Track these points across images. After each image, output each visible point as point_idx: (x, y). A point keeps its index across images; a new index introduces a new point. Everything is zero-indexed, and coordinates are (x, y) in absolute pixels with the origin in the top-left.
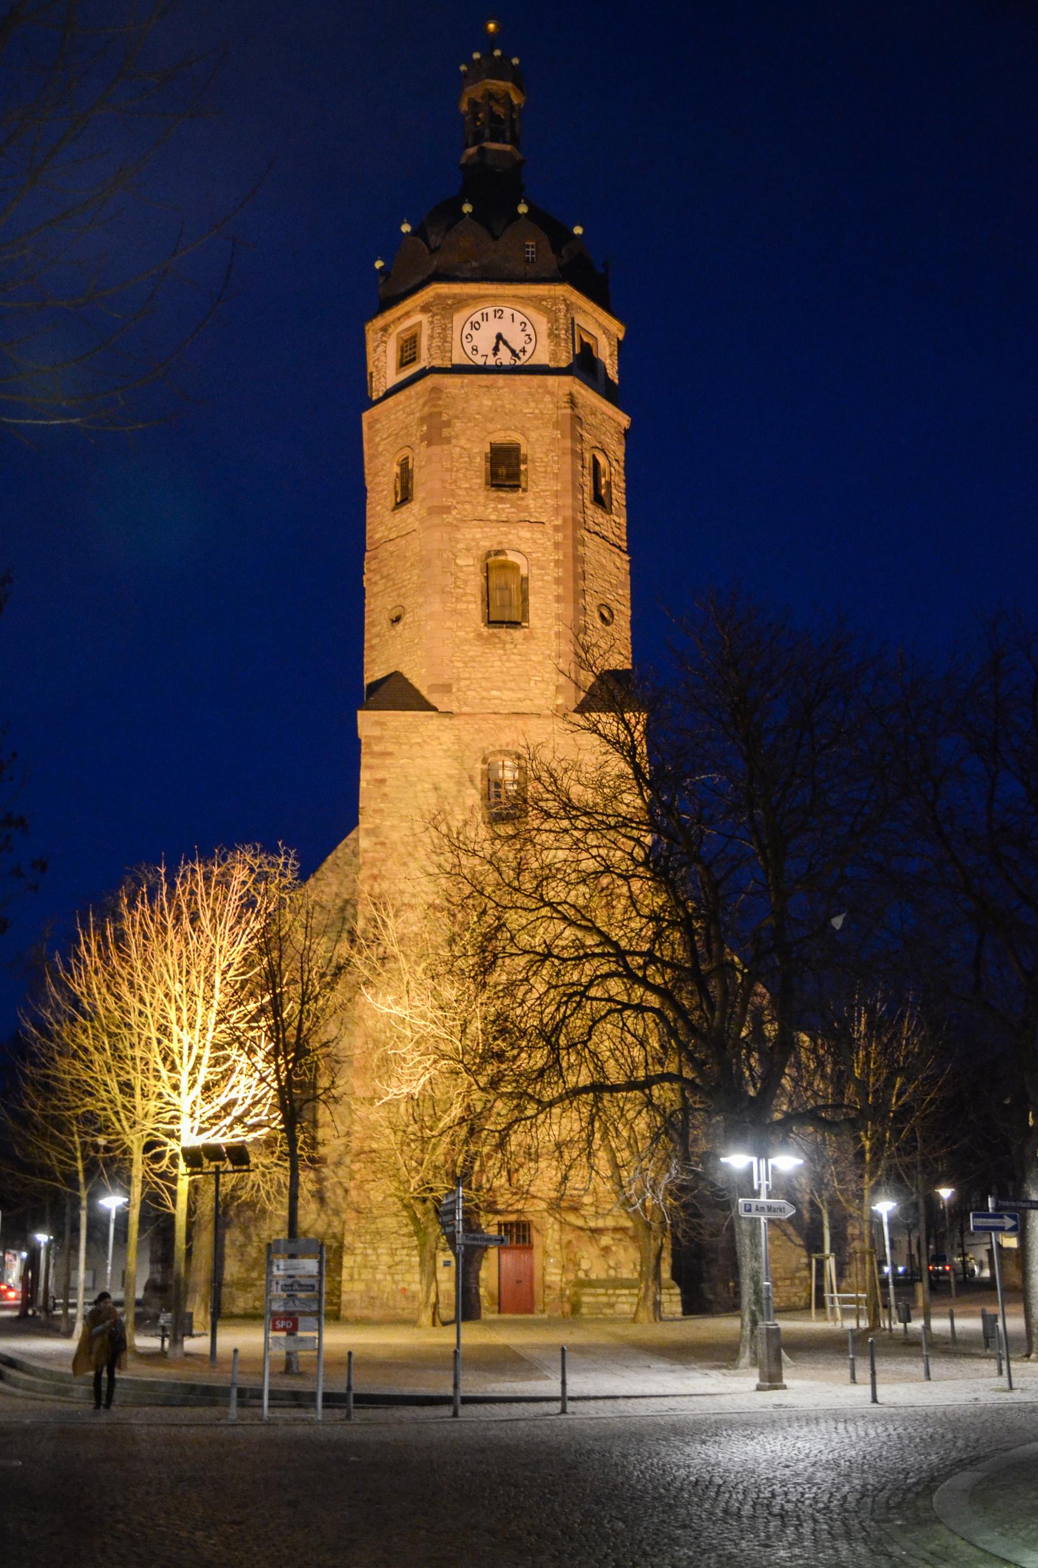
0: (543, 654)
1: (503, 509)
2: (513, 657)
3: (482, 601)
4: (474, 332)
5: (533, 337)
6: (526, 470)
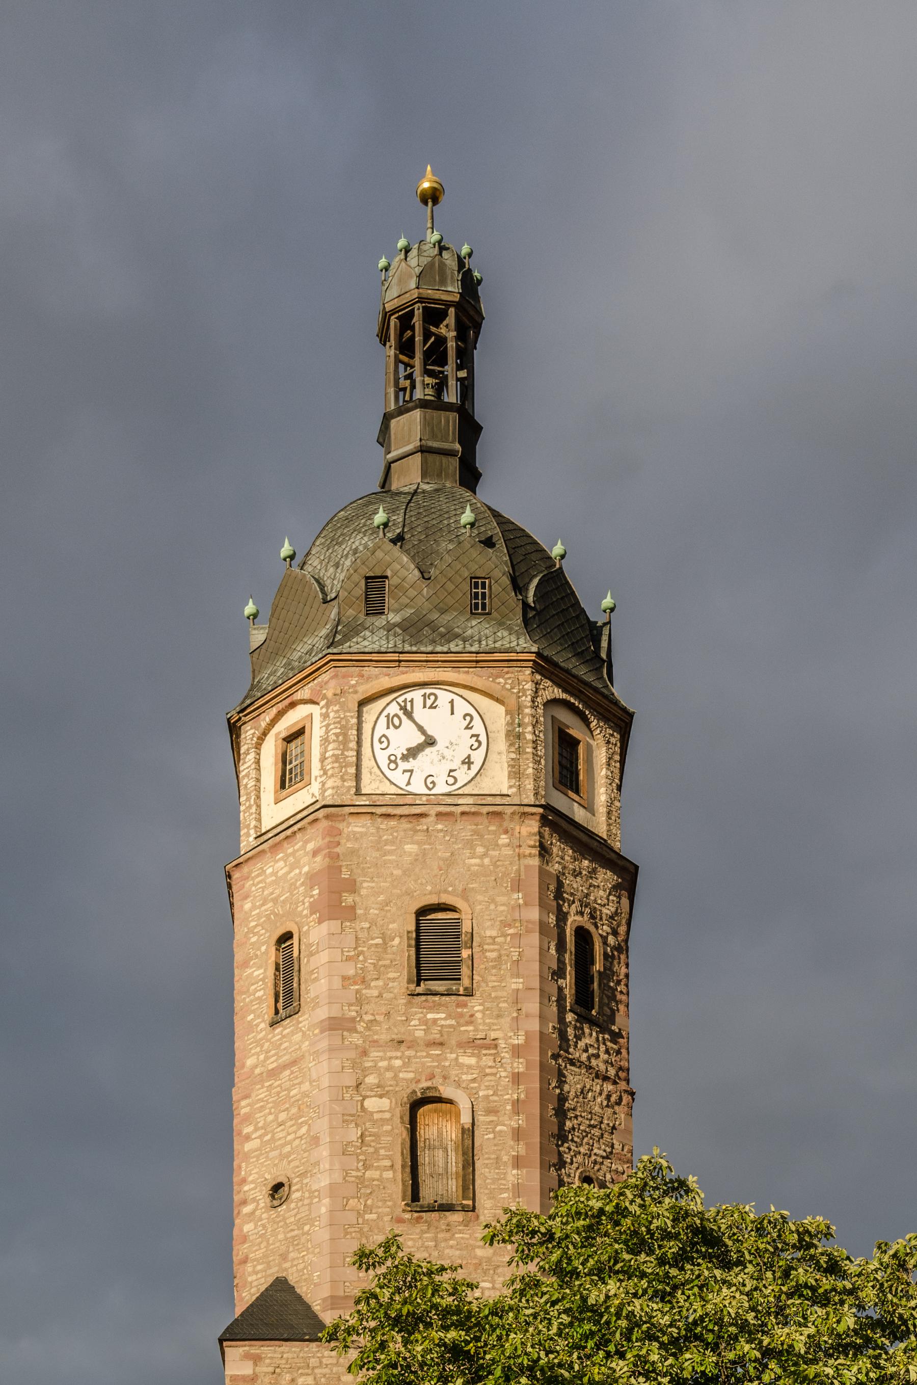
1: (435, 1021)
4: (391, 733)
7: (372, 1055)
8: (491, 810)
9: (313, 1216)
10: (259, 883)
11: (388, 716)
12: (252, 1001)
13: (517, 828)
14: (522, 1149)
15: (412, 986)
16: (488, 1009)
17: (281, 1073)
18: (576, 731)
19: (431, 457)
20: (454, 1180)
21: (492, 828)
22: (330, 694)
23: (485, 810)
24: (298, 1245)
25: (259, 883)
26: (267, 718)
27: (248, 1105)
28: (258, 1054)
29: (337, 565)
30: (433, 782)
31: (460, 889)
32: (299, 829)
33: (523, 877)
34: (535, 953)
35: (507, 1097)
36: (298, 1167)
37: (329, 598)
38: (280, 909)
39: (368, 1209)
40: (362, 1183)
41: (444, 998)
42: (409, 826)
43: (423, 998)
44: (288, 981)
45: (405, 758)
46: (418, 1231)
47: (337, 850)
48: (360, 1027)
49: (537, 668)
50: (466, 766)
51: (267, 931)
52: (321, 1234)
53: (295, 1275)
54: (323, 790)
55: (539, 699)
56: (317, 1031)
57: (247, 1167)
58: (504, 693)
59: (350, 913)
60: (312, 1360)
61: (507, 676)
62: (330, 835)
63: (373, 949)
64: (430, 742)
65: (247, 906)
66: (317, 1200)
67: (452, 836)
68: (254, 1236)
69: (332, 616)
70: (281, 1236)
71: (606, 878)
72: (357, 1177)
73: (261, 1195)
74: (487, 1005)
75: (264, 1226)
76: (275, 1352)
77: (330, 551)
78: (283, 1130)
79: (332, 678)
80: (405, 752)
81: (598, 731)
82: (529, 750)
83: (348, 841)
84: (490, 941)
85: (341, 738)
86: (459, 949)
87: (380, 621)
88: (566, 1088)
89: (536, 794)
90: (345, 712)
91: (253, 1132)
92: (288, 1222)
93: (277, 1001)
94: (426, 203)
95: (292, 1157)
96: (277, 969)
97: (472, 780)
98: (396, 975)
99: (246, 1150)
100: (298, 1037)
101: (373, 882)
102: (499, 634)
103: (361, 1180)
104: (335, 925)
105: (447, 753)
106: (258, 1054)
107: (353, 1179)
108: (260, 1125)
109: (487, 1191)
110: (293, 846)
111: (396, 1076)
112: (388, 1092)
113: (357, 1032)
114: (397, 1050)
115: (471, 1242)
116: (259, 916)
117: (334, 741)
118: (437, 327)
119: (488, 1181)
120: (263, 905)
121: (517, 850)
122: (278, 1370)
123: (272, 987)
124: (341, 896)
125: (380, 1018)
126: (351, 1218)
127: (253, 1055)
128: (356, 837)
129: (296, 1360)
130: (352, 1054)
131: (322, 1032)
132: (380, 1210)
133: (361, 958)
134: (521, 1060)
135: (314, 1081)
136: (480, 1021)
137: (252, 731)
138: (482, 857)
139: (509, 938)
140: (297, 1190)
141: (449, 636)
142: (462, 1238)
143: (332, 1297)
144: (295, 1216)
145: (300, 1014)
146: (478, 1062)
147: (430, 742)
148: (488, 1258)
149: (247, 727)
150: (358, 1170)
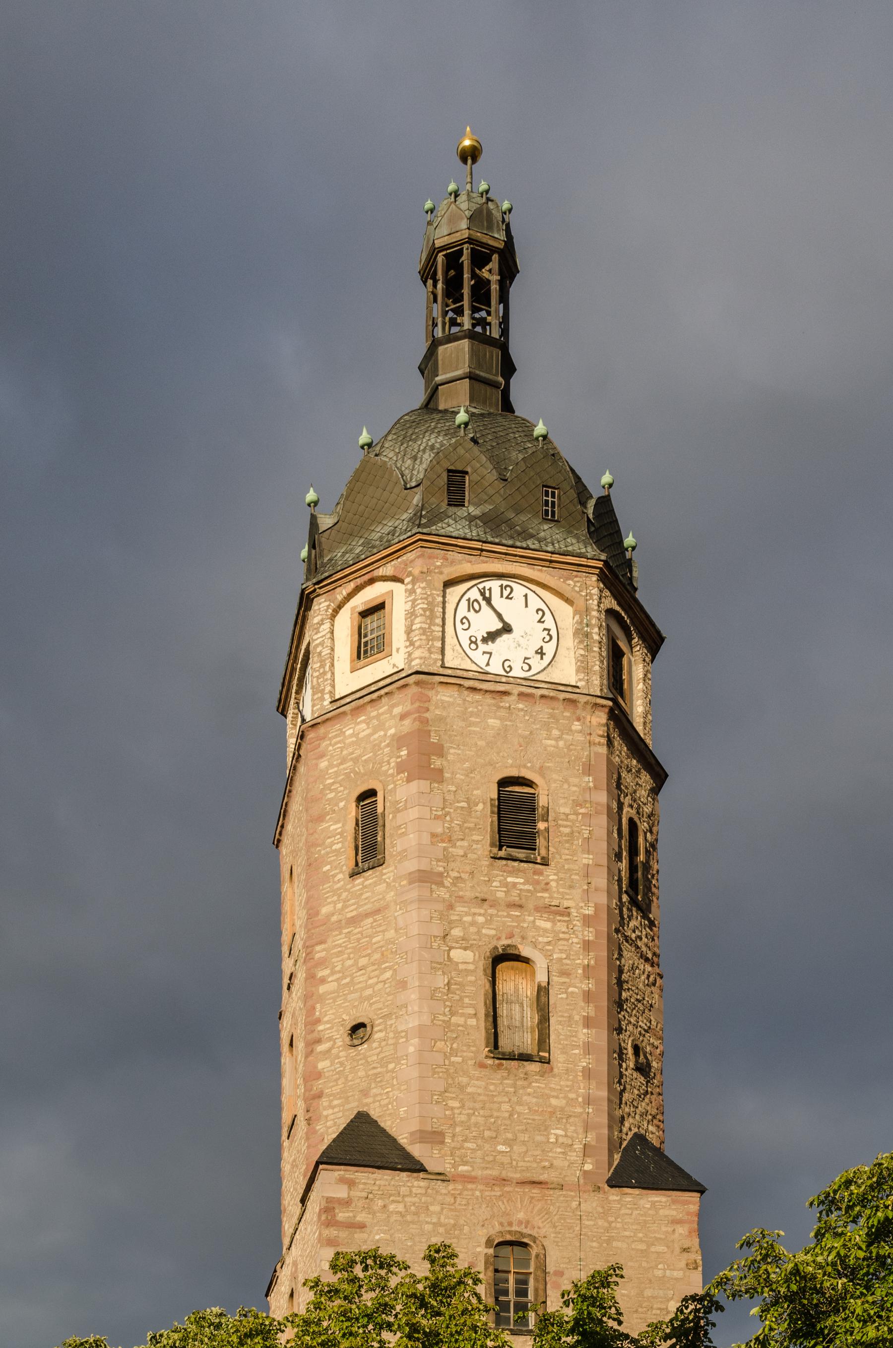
0: (565, 1097)
1: (515, 885)
3: (486, 1015)
4: (471, 615)
5: (554, 633)
6: (547, 830)
7: (458, 909)
8: (565, 696)
9: (399, 1054)
10: (336, 743)
11: (469, 600)
12: (328, 853)
13: (588, 717)
14: (591, 1011)
15: (495, 850)
16: (561, 879)
17: (362, 921)
18: (623, 644)
19: (477, 385)
20: (529, 1034)
21: (567, 714)
22: (416, 572)
23: (562, 696)
24: (381, 1081)
25: (336, 743)
26: (344, 591)
27: (324, 950)
28: (335, 903)
29: (415, 458)
30: (510, 666)
31: (538, 766)
32: (386, 694)
33: (593, 762)
34: (603, 833)
35: (578, 961)
36: (381, 1009)
37: (408, 486)
38: (361, 768)
39: (454, 1052)
40: (448, 1027)
41: (522, 864)
42: (493, 701)
43: (504, 862)
45: (485, 640)
46: (499, 1076)
47: (427, 715)
48: (447, 882)
49: (602, 577)
50: (539, 656)
51: (345, 788)
52: (409, 1072)
53: (377, 1110)
54: (409, 658)
55: (602, 605)
56: (404, 883)
57: (322, 1008)
58: (574, 594)
59: (438, 776)
60: (403, 1189)
61: (576, 579)
62: (421, 701)
63: (459, 811)
64: (507, 629)
65: (323, 764)
66: (404, 1040)
67: (531, 716)
68: (331, 1073)
69: (415, 502)
70: (361, 1074)
71: (646, 779)
72: (443, 1021)
73: (341, 1036)
74: (561, 875)
75: (342, 1064)
76: (368, 1178)
77: (405, 445)
78: (363, 974)
79: (418, 557)
80: (485, 635)
81: (638, 648)
82: (596, 649)
83: (436, 708)
84: (564, 817)
85: (428, 613)
86: (534, 821)
87: (462, 512)
88: (623, 961)
89: (601, 690)
90: (431, 590)
91: (329, 976)
92: (369, 1059)
93: (357, 854)
94: (464, 161)
95: (374, 1000)
96: (357, 824)
97: (544, 669)
98: (480, 838)
99: (321, 991)
101: (459, 749)
102: (569, 540)
103: (447, 1023)
104: (424, 785)
105: (522, 641)
106: (335, 903)
107: (441, 1023)
108: (337, 969)
109: (560, 1046)
110: (378, 710)
111: (478, 932)
112: (472, 945)
113: (444, 887)
114: (481, 907)
115: (547, 1091)
117: (421, 615)
118: (480, 270)
119: (561, 1037)
120: (341, 764)
121: (588, 737)
122: (370, 1196)
123: (353, 840)
124: (430, 759)
125: (465, 876)
126: (439, 1059)
127: (330, 903)
128: (444, 706)
129: (388, 1188)
130: (440, 907)
131: (410, 883)
132: (465, 1054)
133: (448, 818)
134: (591, 929)
135: (401, 929)
136: (555, 889)
137: (327, 603)
138: (557, 739)
139: (580, 817)
140: (380, 1031)
141: (525, 535)
142: (539, 1087)
143: (421, 1131)
144: (378, 1055)
145: (384, 866)
146: (552, 927)
147: (507, 629)
148: (561, 1107)
149: (321, 599)
150: (444, 1014)
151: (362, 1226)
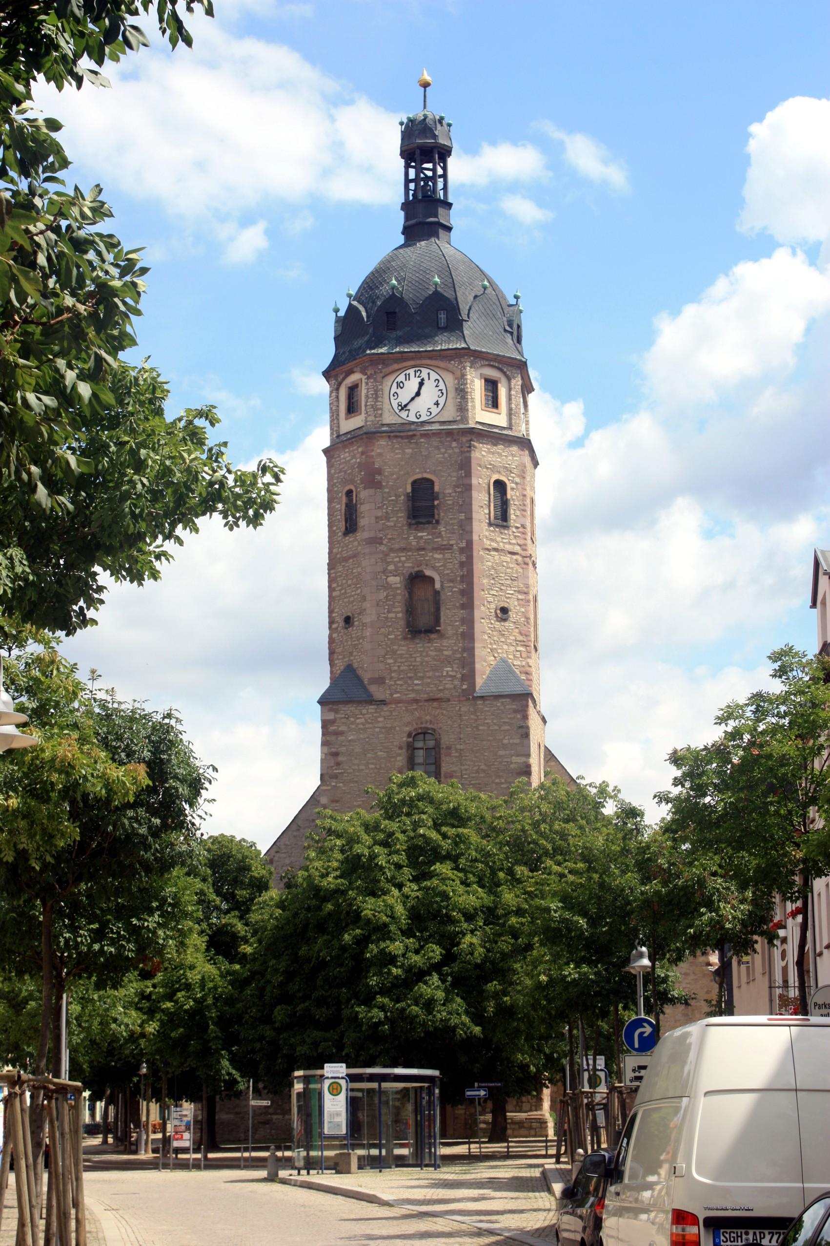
1: (422, 537)
2: (430, 653)
4: (399, 391)
5: (444, 391)
44: (351, 514)
59: (378, 485)
100: (356, 543)
116: (338, 478)
130: (381, 556)
151: (342, 733)
